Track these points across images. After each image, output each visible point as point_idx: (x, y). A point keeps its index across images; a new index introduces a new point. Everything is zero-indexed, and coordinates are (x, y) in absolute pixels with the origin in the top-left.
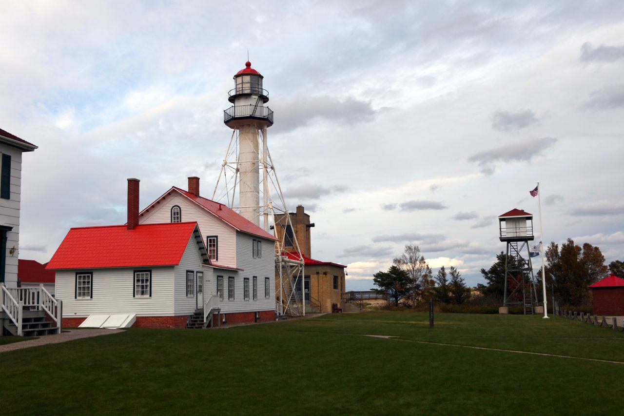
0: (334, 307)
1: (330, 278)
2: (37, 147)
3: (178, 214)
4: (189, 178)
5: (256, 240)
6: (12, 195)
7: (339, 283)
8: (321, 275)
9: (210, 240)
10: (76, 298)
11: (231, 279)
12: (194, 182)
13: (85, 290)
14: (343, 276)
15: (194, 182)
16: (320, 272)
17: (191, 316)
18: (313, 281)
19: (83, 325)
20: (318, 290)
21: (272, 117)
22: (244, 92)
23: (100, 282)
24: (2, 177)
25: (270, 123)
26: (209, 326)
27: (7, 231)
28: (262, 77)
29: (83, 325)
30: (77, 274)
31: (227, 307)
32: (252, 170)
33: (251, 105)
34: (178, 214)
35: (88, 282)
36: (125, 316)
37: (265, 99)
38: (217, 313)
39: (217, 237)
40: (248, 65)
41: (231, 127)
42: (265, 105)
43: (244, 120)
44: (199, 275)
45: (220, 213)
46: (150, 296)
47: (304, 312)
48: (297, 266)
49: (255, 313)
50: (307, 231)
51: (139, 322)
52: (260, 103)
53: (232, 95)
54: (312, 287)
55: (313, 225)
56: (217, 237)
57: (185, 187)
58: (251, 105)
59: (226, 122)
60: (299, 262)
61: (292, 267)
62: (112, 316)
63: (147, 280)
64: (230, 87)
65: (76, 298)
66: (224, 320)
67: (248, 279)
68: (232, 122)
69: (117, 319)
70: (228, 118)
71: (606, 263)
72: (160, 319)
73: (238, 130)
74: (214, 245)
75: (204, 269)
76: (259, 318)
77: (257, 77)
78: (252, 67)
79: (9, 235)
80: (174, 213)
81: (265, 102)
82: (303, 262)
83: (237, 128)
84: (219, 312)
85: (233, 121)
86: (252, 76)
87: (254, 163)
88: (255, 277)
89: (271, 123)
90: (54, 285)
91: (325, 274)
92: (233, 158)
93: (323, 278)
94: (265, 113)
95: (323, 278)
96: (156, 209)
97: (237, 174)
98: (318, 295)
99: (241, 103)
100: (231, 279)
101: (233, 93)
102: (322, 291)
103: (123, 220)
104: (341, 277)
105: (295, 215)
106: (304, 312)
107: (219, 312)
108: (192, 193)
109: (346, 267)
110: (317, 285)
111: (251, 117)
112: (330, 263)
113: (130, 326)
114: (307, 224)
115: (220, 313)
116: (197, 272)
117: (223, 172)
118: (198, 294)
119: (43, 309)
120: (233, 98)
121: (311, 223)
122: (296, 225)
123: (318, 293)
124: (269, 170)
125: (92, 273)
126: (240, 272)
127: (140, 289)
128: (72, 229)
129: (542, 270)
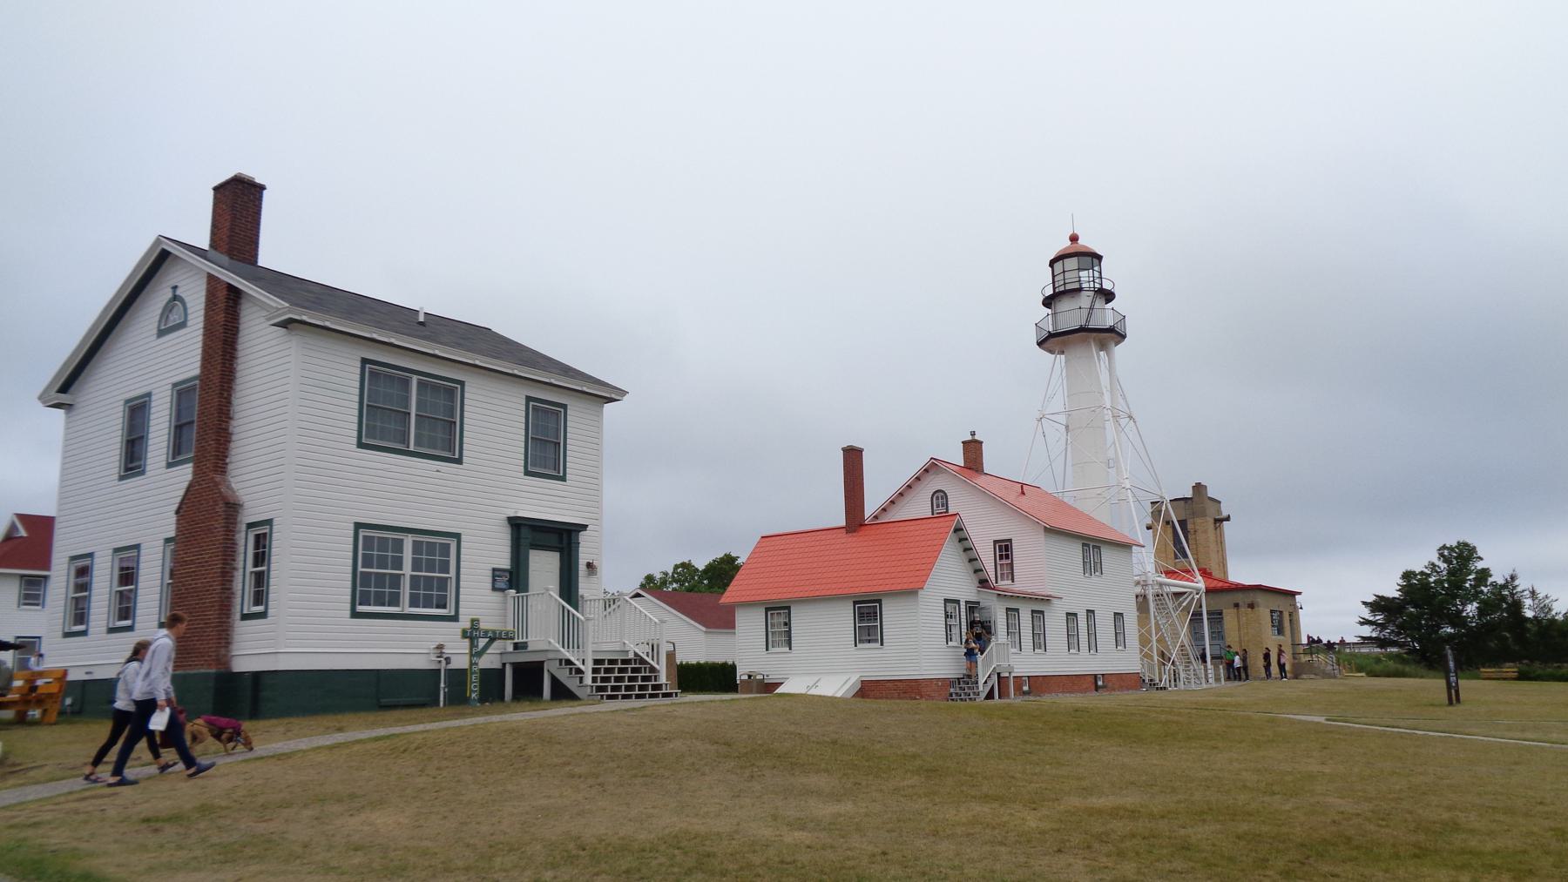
1: (1264, 613)
2: (149, 395)
7: (1287, 624)
12: (973, 448)
13: (780, 631)
15: (973, 448)
19: (779, 690)
23: (802, 620)
26: (990, 696)
28: (1100, 258)
32: (1081, 425)
36: (845, 678)
37: (1108, 296)
40: (1074, 239)
41: (1051, 352)
42: (1110, 305)
45: (1024, 502)
51: (868, 690)
52: (1099, 303)
59: (1040, 344)
61: (1178, 595)
66: (1026, 688)
68: (1050, 341)
69: (836, 685)
70: (1045, 334)
71: (1490, 580)
76: (1104, 687)
81: (1108, 301)
83: (1063, 353)
88: (1090, 612)
89: (1123, 337)
91: (1251, 606)
92: (1058, 404)
94: (1109, 323)
96: (907, 498)
99: (1065, 305)
101: (1049, 291)
103: (836, 516)
111: (1082, 329)
121: (1225, 514)
122: (1190, 522)
124: (1124, 422)
126: (1055, 601)
129: (22, 576)
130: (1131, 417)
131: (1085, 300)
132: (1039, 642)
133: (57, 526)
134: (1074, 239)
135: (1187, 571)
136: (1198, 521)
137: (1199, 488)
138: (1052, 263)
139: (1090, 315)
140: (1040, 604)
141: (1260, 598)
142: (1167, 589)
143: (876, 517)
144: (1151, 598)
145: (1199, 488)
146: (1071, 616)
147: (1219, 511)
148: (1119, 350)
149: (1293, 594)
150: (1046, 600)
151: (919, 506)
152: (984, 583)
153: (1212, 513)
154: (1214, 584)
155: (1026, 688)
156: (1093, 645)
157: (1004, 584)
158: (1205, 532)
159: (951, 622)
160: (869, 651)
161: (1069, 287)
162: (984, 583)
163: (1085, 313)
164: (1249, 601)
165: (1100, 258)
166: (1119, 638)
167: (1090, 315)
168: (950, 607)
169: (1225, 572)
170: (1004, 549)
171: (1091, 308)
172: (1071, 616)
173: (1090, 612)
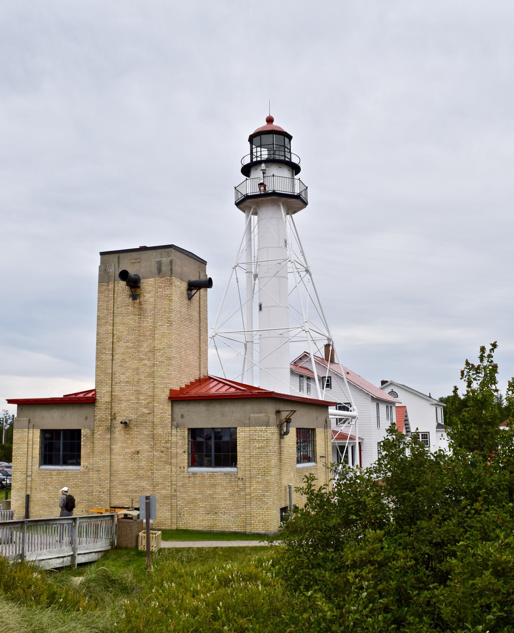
9: (427, 445)
21: (306, 194)
22: (262, 159)
33: (273, 176)
37: (296, 169)
39: (429, 432)
43: (179, 254)
56: (429, 432)
58: (273, 176)
59: (238, 204)
64: (243, 153)
68: (245, 203)
97: (255, 280)
101: (247, 161)
117: (234, 276)
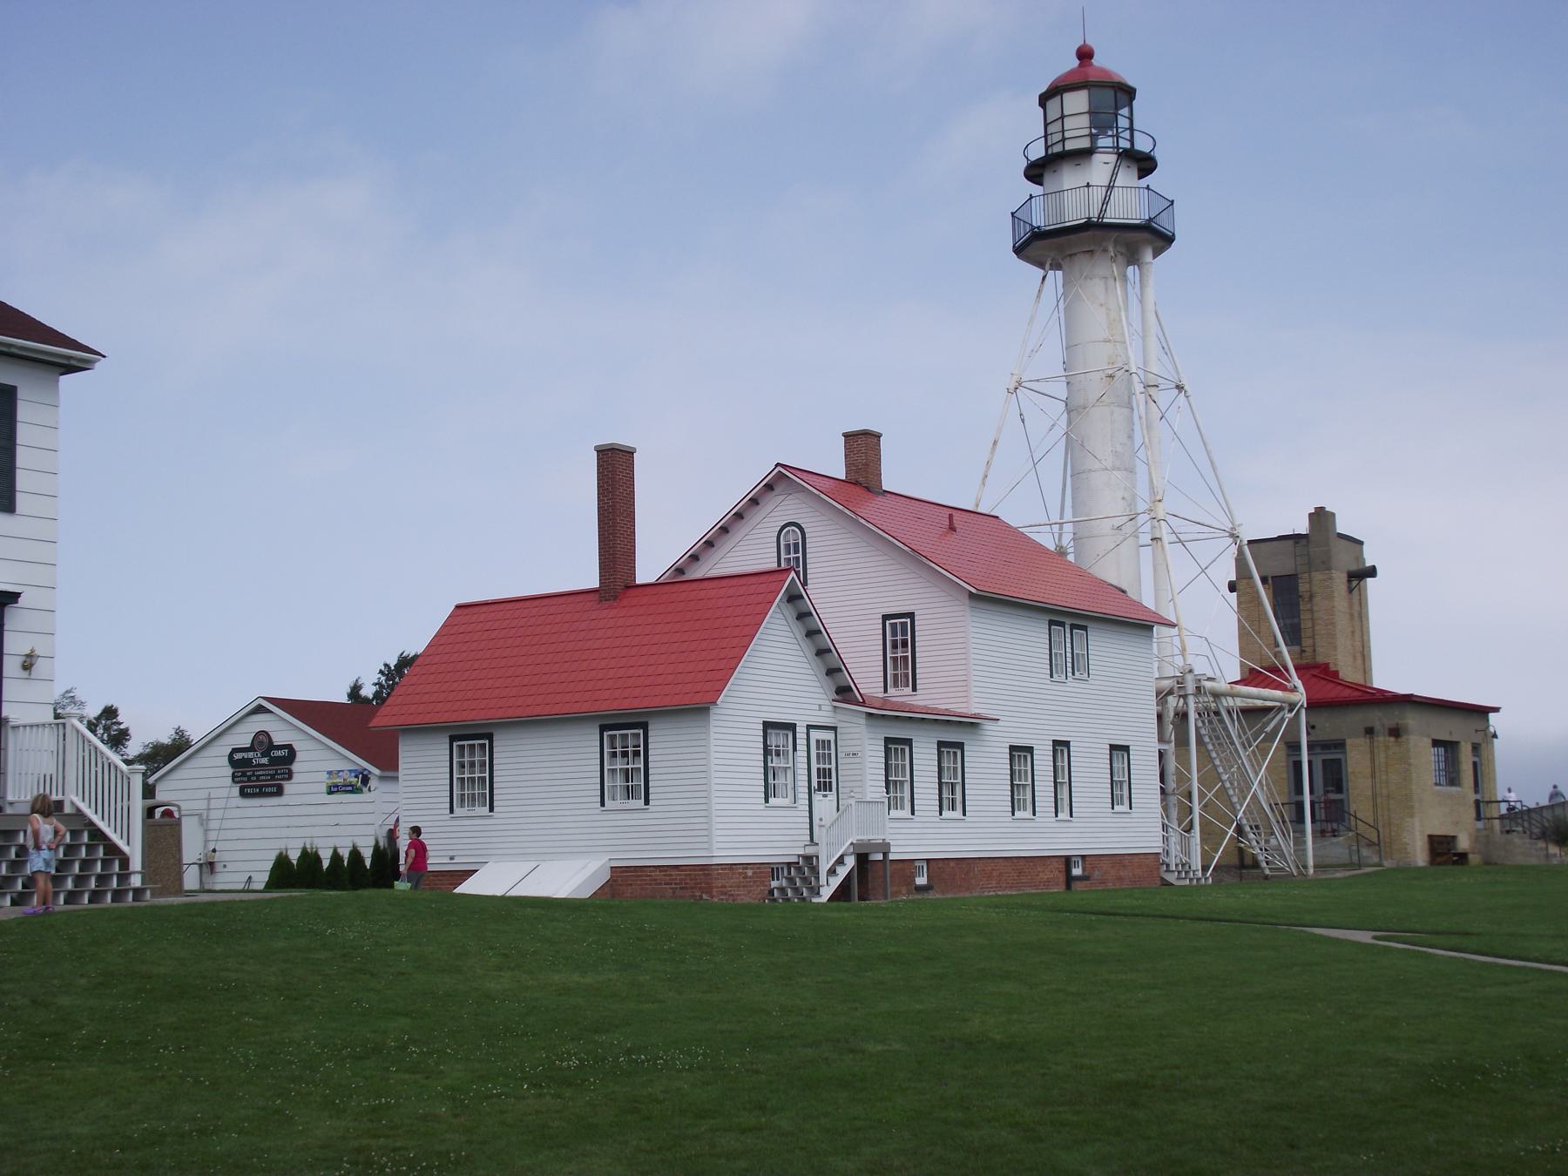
0: (1442, 848)
3: (796, 551)
4: (846, 435)
5: (1062, 624)
6: (21, 501)
8: (1381, 739)
9: (894, 626)
10: (452, 811)
11: (949, 749)
12: (863, 447)
13: (475, 788)
14: (1483, 744)
15: (863, 447)
16: (1378, 727)
17: (789, 864)
18: (1356, 759)
19: (466, 888)
20: (1373, 787)
24: (599, 466)
25: (1164, 240)
27: (5, 605)
29: (466, 888)
30: (452, 739)
31: (919, 836)
32: (1090, 405)
33: (1088, 185)
34: (796, 551)
35: (483, 764)
37: (1145, 164)
38: (880, 857)
40: (1085, 55)
41: (1041, 265)
44: (816, 735)
46: (647, 802)
47: (1311, 862)
48: (1281, 709)
49: (1068, 861)
50: (1350, 591)
51: (623, 880)
52: (1127, 177)
53: (1033, 158)
54: (1351, 777)
55: (1372, 572)
56: (911, 615)
57: (836, 467)
58: (1088, 185)
59: (1019, 250)
60: (1278, 693)
62: (543, 865)
63: (637, 754)
64: (1025, 132)
65: (452, 811)
67: (1030, 750)
68: (1042, 245)
69: (567, 877)
70: (1025, 233)
72: (674, 873)
73: (1059, 273)
74: (904, 644)
75: (840, 717)
77: (1115, 96)
78: (1097, 61)
79: (14, 618)
80: (788, 546)
82: (1301, 697)
83: (1056, 266)
84: (885, 854)
85: (1037, 244)
86: (1095, 91)
87: (1111, 376)
88: (1061, 746)
89: (1167, 240)
90: (397, 778)
91: (1396, 732)
93: (1387, 747)
95: (1387, 747)
98: (1375, 806)
99: (1068, 178)
100: (949, 749)
101: (1037, 152)
102: (1385, 792)
103: (589, 578)
104: (1476, 748)
105: (1304, 542)
106: (1311, 862)
107: (885, 854)
108: (856, 483)
109: (1496, 710)
110: (1368, 771)
111: (1088, 226)
112: (1412, 695)
113: (586, 894)
114: (1353, 567)
115: (891, 857)
116: (809, 727)
118: (817, 797)
119: (78, 810)
120: (1037, 171)
123: (1374, 797)
125: (490, 737)
126: (988, 726)
127: (619, 781)
128: (458, 607)
130: (1180, 388)
131: (1100, 168)
132: (951, 794)
133: (638, 459)
134: (1085, 55)
135: (1275, 670)
136: (1318, 576)
137: (1321, 517)
138: (1044, 100)
139: (1105, 202)
140: (955, 733)
141: (1412, 719)
142: (1230, 702)
143: (680, 571)
144: (1192, 716)
145: (1321, 517)
146: (1021, 753)
147: (1360, 557)
148: (1159, 266)
149: (1482, 712)
150: (971, 724)
151: (753, 552)
152: (844, 693)
153: (1343, 562)
154: (1333, 692)
155: (921, 880)
156: (1063, 799)
157: (901, 695)
158: (1330, 597)
159: (775, 762)
160: (626, 817)
161: (1070, 146)
162: (844, 693)
163: (1098, 195)
164: (1391, 723)
165: (1128, 93)
166: (1120, 790)
167: (1105, 202)
168: (776, 739)
169: (1366, 670)
170: (900, 633)
171: (1110, 187)
172: (1021, 753)
173: (1061, 746)
